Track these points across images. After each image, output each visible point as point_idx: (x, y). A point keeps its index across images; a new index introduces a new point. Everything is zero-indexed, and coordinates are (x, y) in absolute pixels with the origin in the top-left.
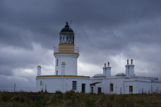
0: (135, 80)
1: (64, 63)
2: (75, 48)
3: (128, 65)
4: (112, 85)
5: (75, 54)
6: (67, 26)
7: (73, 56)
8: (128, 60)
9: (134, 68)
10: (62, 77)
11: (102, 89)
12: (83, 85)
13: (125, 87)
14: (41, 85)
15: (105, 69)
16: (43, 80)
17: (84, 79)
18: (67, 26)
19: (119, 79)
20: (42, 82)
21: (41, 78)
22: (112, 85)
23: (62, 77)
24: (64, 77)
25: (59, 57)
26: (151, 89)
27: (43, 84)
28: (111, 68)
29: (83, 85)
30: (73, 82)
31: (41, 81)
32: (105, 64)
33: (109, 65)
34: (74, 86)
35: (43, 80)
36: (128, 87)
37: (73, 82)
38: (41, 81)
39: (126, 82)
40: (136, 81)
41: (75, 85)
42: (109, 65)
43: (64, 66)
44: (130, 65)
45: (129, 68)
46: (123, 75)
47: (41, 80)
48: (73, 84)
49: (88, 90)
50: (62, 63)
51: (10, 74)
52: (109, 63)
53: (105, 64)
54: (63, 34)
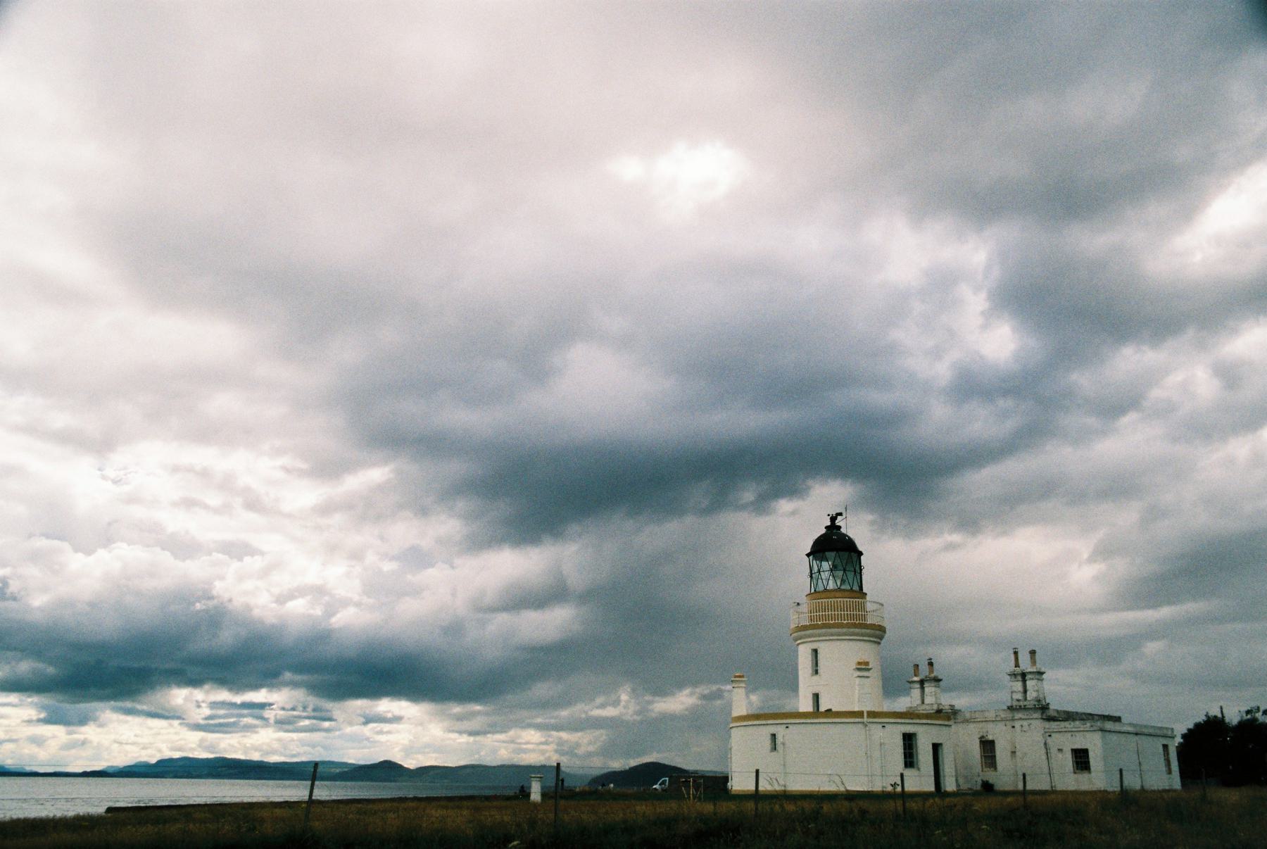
1: (867, 664)
2: (869, 607)
4: (988, 746)
5: (872, 626)
6: (833, 528)
7: (862, 635)
10: (865, 720)
11: (1091, 754)
13: (1053, 751)
14: (774, 748)
15: (918, 686)
16: (780, 732)
19: (1025, 723)
20: (779, 739)
22: (988, 746)
23: (865, 720)
26: (1046, 770)
27: (783, 744)
28: (1042, 673)
31: (774, 736)
33: (1034, 662)
35: (780, 732)
36: (1069, 756)
38: (774, 736)
42: (1034, 662)
43: (865, 674)
47: (773, 730)
50: (859, 663)
51: (652, 711)
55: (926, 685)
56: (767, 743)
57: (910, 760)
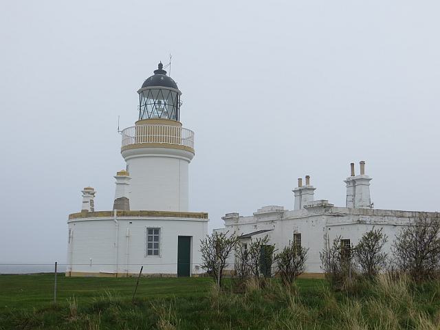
0: (356, 219)
3: (352, 178)
7: (134, 154)
8: (352, 165)
9: (189, 162)
12: (184, 243)
15: (352, 184)
17: (100, 222)
18: (160, 71)
19: (314, 219)
21: (98, 218)
24: (119, 218)
25: (184, 161)
28: (314, 189)
29: (184, 243)
30: (150, 231)
32: (300, 180)
34: (153, 235)
37: (150, 231)
39: (332, 228)
40: (360, 222)
41: (157, 239)
42: (308, 182)
44: (359, 177)
45: (354, 186)
46: (110, 212)
48: (150, 239)
49: (198, 262)
52: (308, 177)
53: (300, 180)
54: (150, 96)
55: (357, 183)
56: (143, 236)
57: (153, 247)
